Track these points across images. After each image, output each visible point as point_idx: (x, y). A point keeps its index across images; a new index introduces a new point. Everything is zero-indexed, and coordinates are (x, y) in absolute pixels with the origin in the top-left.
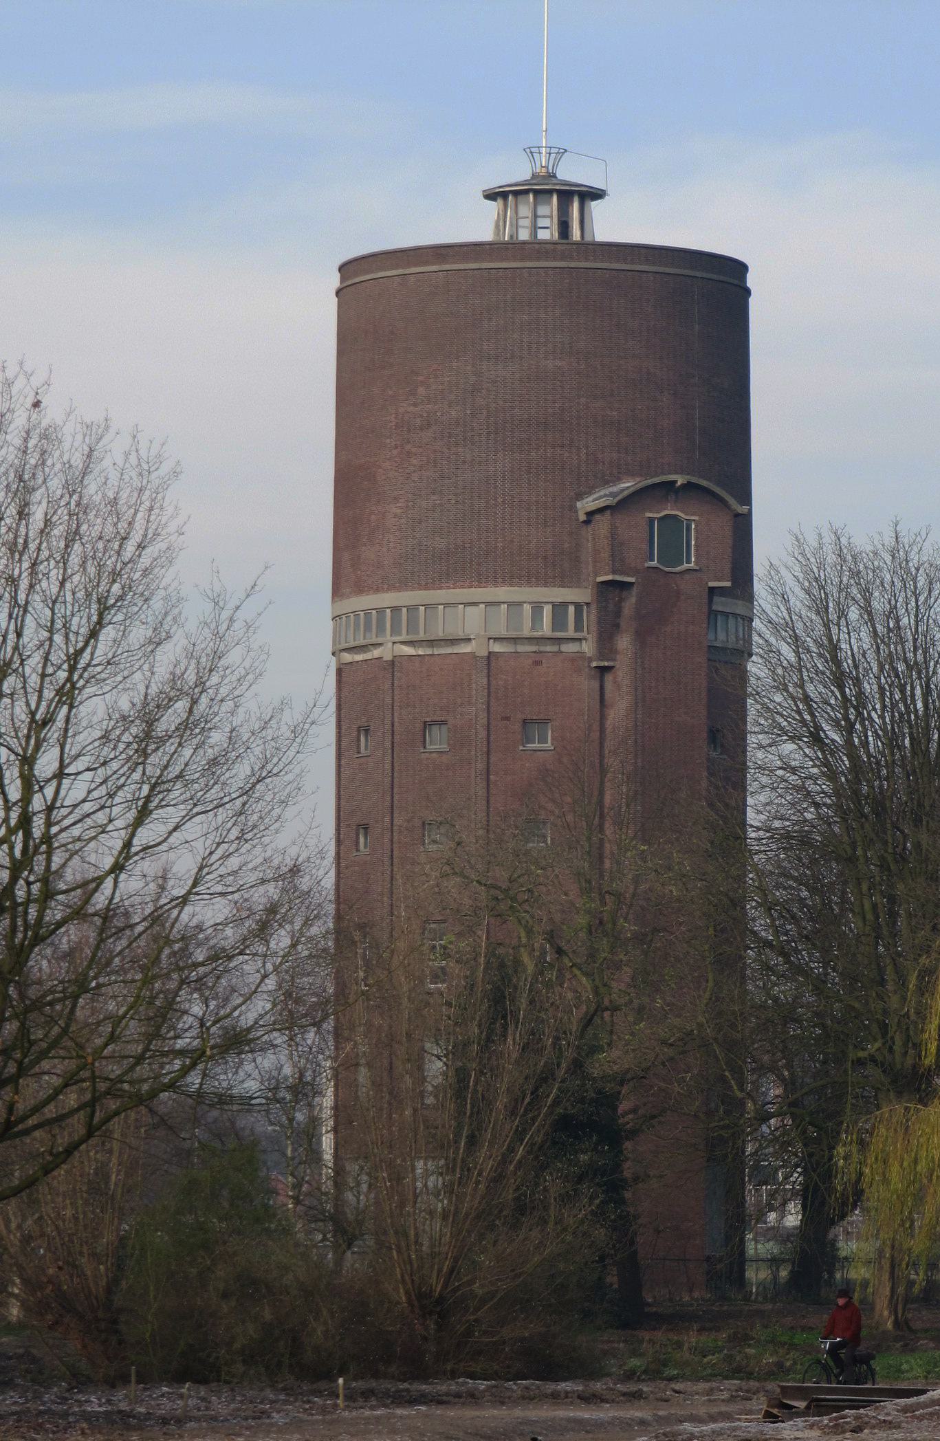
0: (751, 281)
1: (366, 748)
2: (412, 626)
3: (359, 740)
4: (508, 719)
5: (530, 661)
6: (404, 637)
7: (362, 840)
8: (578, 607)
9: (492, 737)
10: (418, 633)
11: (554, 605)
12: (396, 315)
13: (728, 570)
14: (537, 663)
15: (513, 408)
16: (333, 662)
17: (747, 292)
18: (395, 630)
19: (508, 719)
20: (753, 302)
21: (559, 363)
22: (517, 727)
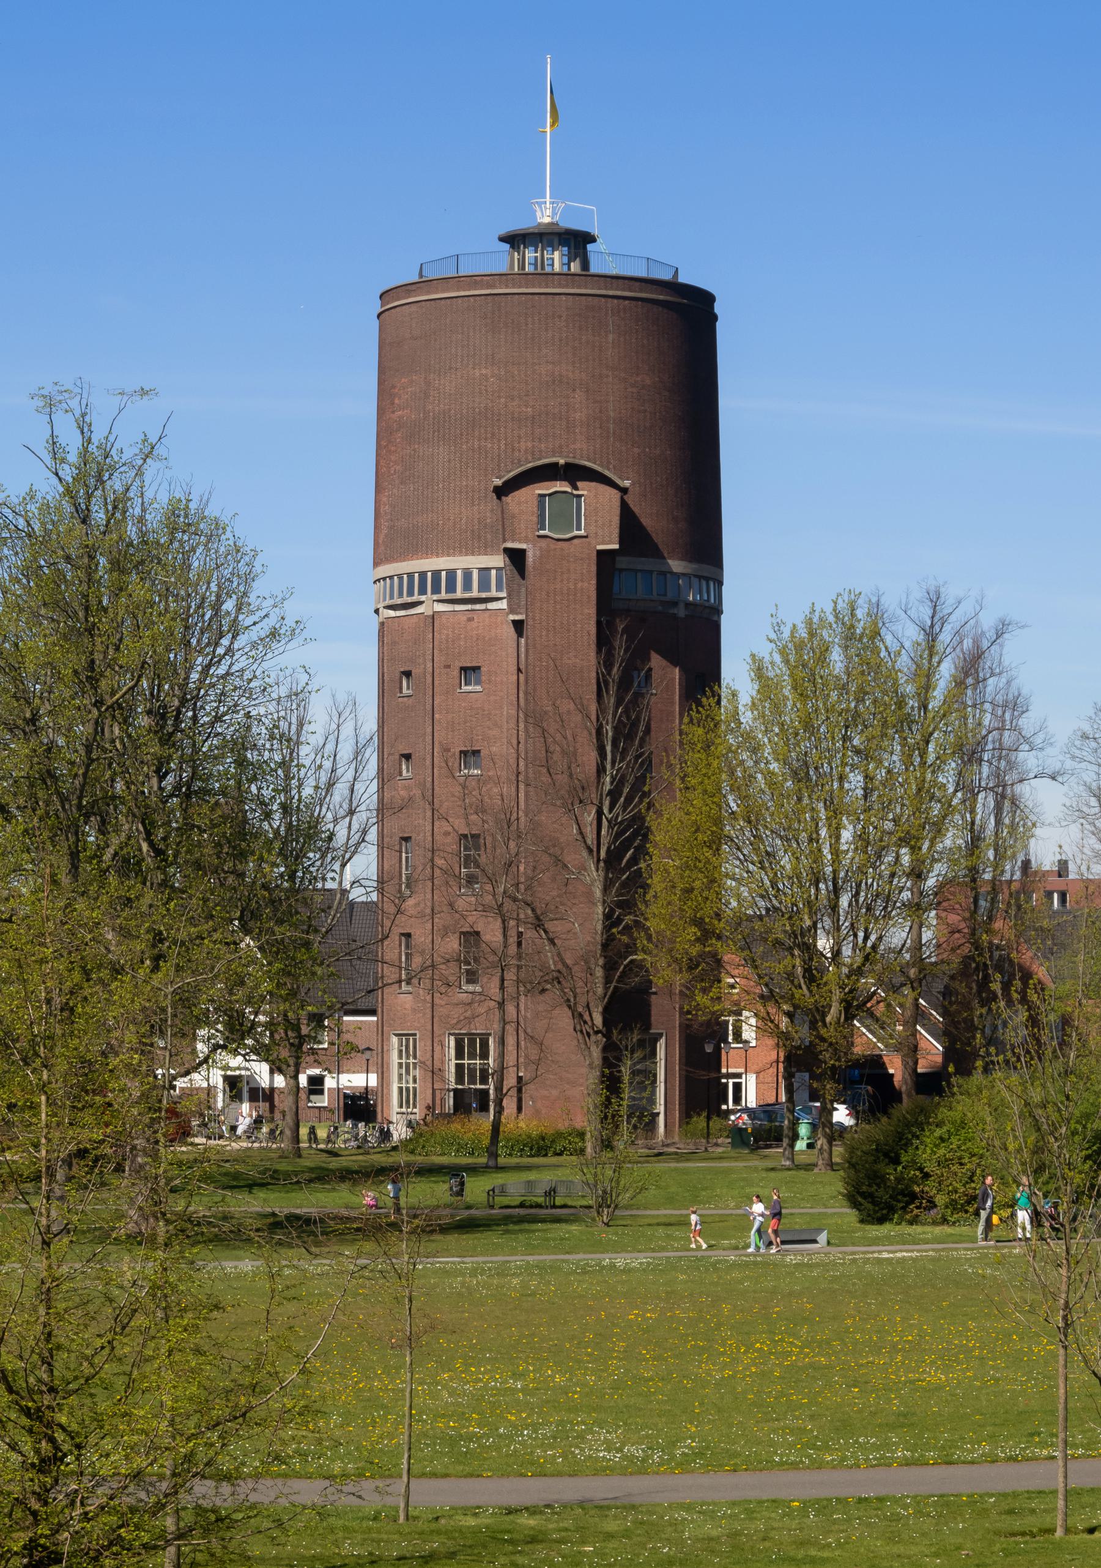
0: (717, 309)
1: (408, 688)
2: (451, 588)
3: (401, 683)
4: (448, 667)
5: (465, 618)
6: (443, 595)
7: (404, 767)
8: (498, 569)
9: (436, 683)
10: (489, 590)
11: (480, 569)
12: (414, 324)
13: (617, 539)
14: (470, 620)
15: (450, 410)
16: (374, 622)
17: (715, 318)
18: (436, 590)
19: (448, 667)
20: (720, 326)
21: (484, 371)
22: (456, 673)
